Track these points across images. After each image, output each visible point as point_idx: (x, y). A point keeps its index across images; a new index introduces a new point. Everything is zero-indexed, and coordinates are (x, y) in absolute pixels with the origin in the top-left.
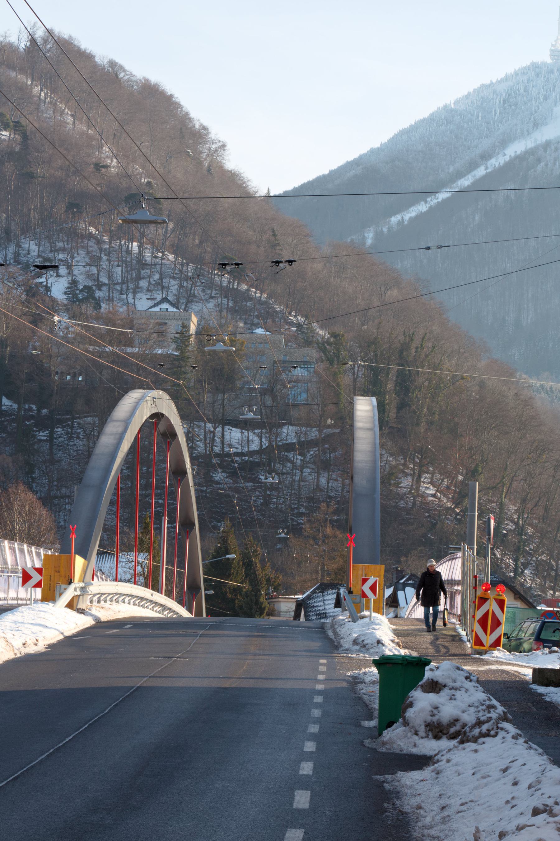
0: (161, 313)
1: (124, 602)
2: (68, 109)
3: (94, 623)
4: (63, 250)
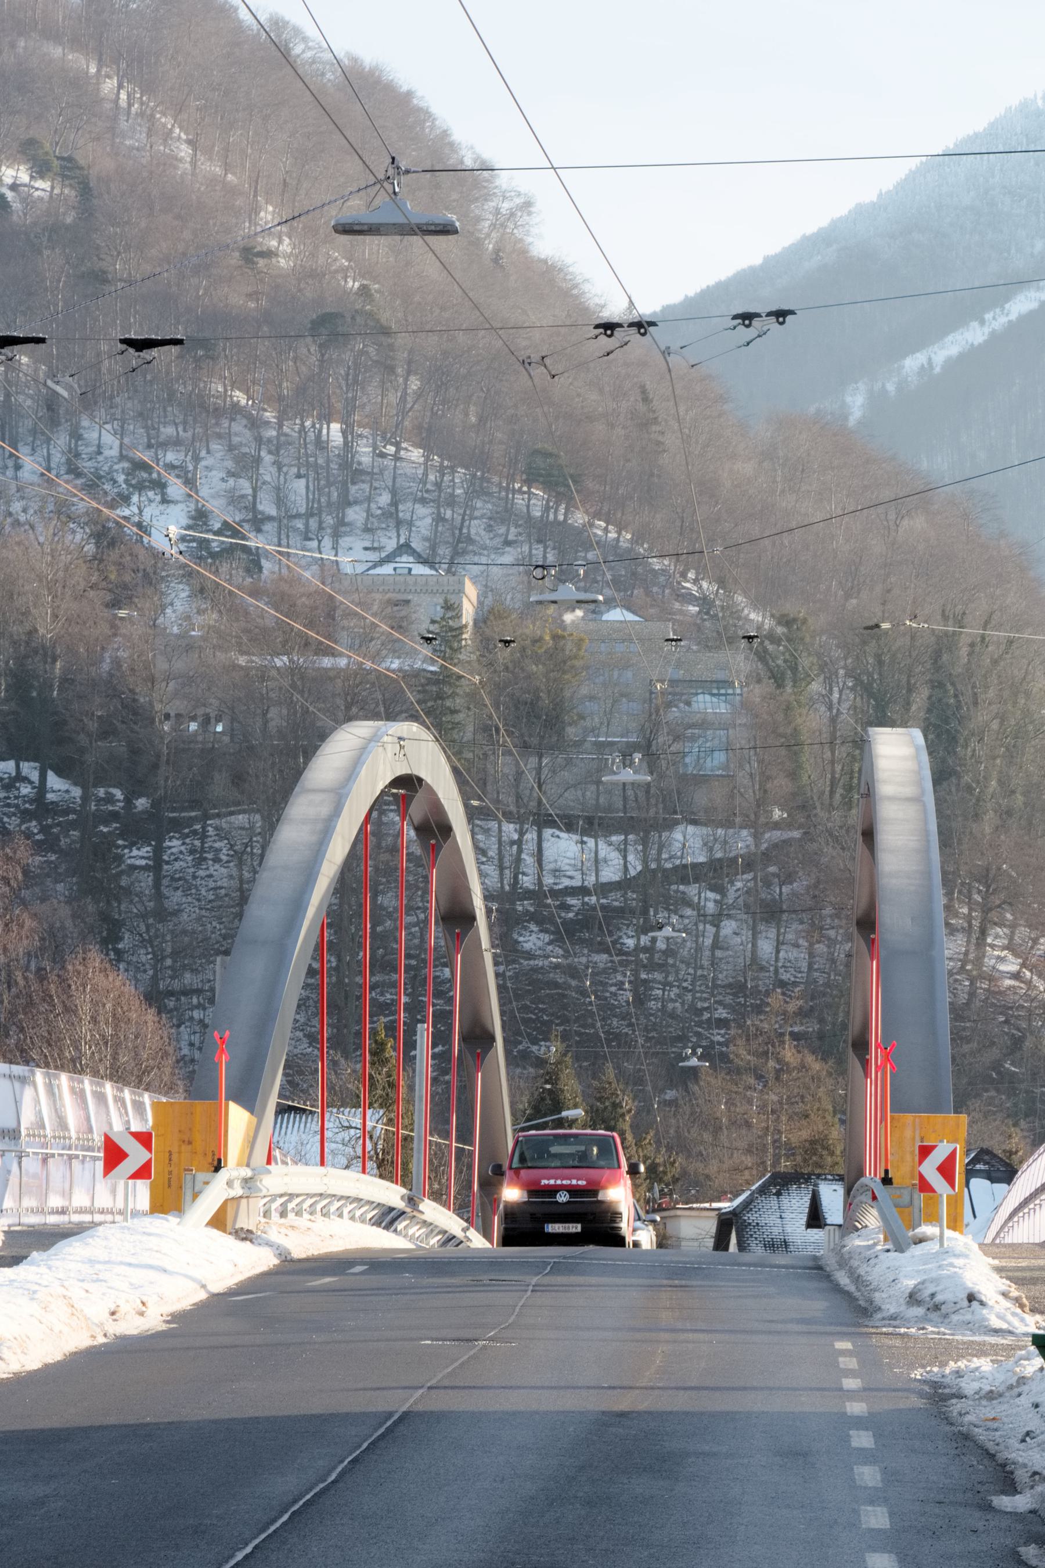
0: (398, 578)
1: (341, 1216)
2: (181, 128)
3: (276, 1262)
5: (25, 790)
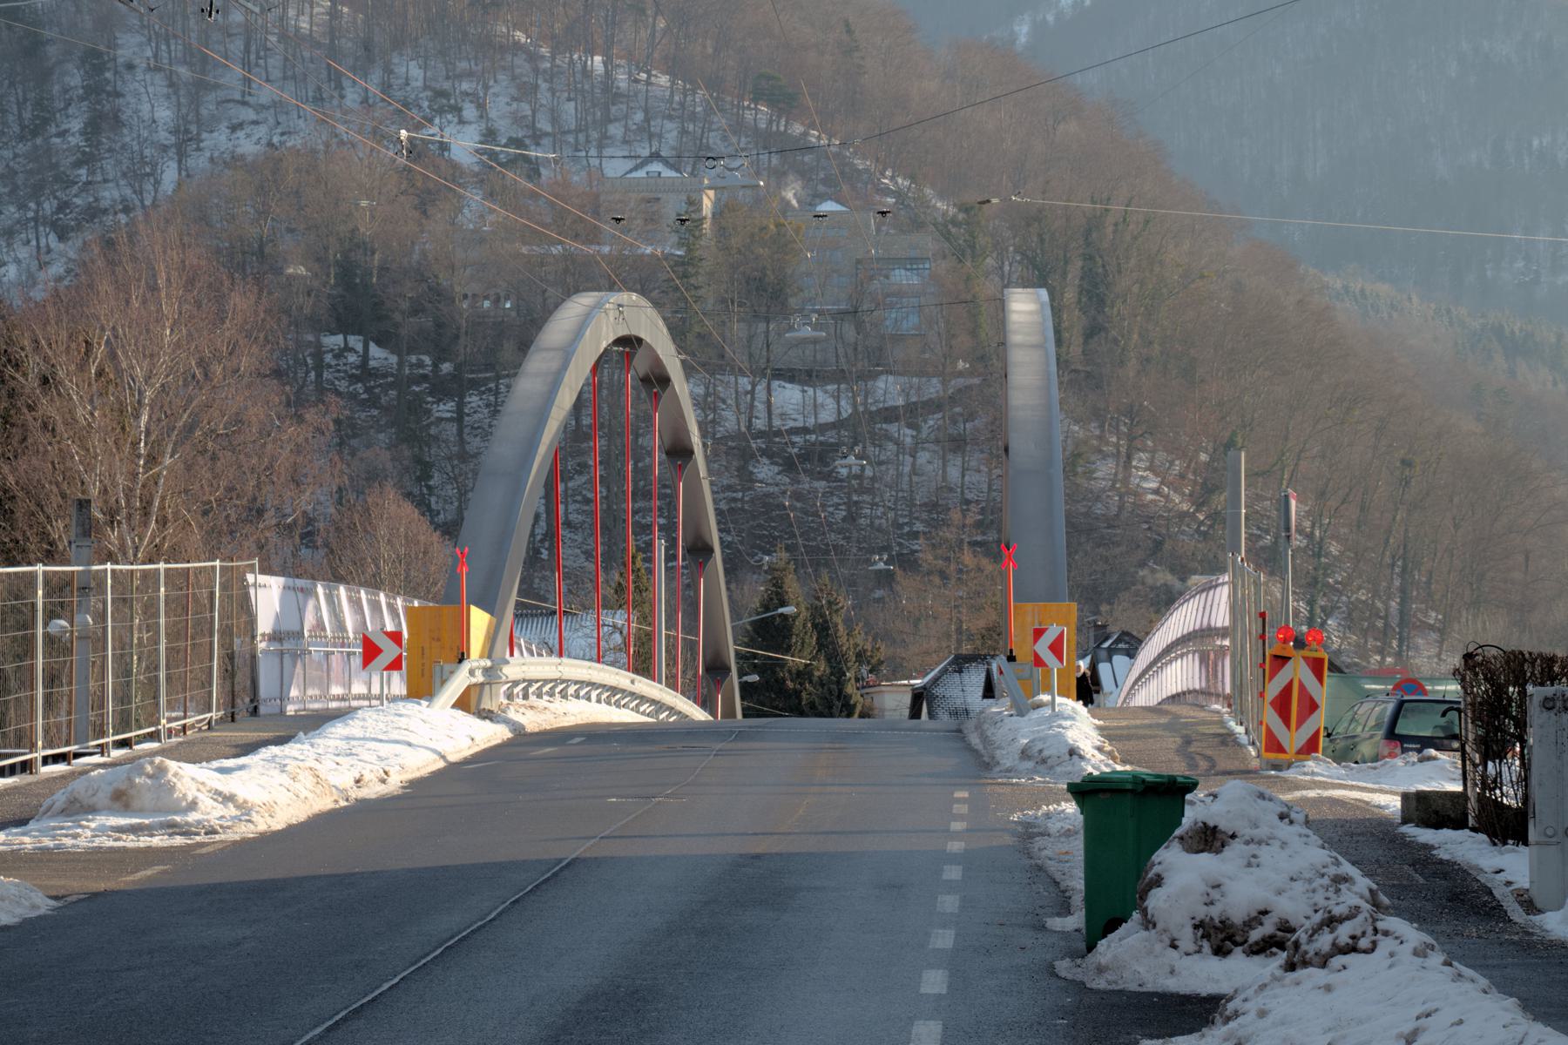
3: (510, 735)
4: (470, 74)
5: (352, 358)
